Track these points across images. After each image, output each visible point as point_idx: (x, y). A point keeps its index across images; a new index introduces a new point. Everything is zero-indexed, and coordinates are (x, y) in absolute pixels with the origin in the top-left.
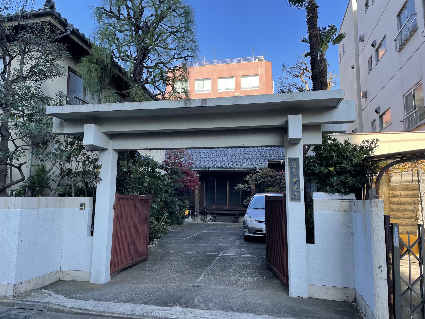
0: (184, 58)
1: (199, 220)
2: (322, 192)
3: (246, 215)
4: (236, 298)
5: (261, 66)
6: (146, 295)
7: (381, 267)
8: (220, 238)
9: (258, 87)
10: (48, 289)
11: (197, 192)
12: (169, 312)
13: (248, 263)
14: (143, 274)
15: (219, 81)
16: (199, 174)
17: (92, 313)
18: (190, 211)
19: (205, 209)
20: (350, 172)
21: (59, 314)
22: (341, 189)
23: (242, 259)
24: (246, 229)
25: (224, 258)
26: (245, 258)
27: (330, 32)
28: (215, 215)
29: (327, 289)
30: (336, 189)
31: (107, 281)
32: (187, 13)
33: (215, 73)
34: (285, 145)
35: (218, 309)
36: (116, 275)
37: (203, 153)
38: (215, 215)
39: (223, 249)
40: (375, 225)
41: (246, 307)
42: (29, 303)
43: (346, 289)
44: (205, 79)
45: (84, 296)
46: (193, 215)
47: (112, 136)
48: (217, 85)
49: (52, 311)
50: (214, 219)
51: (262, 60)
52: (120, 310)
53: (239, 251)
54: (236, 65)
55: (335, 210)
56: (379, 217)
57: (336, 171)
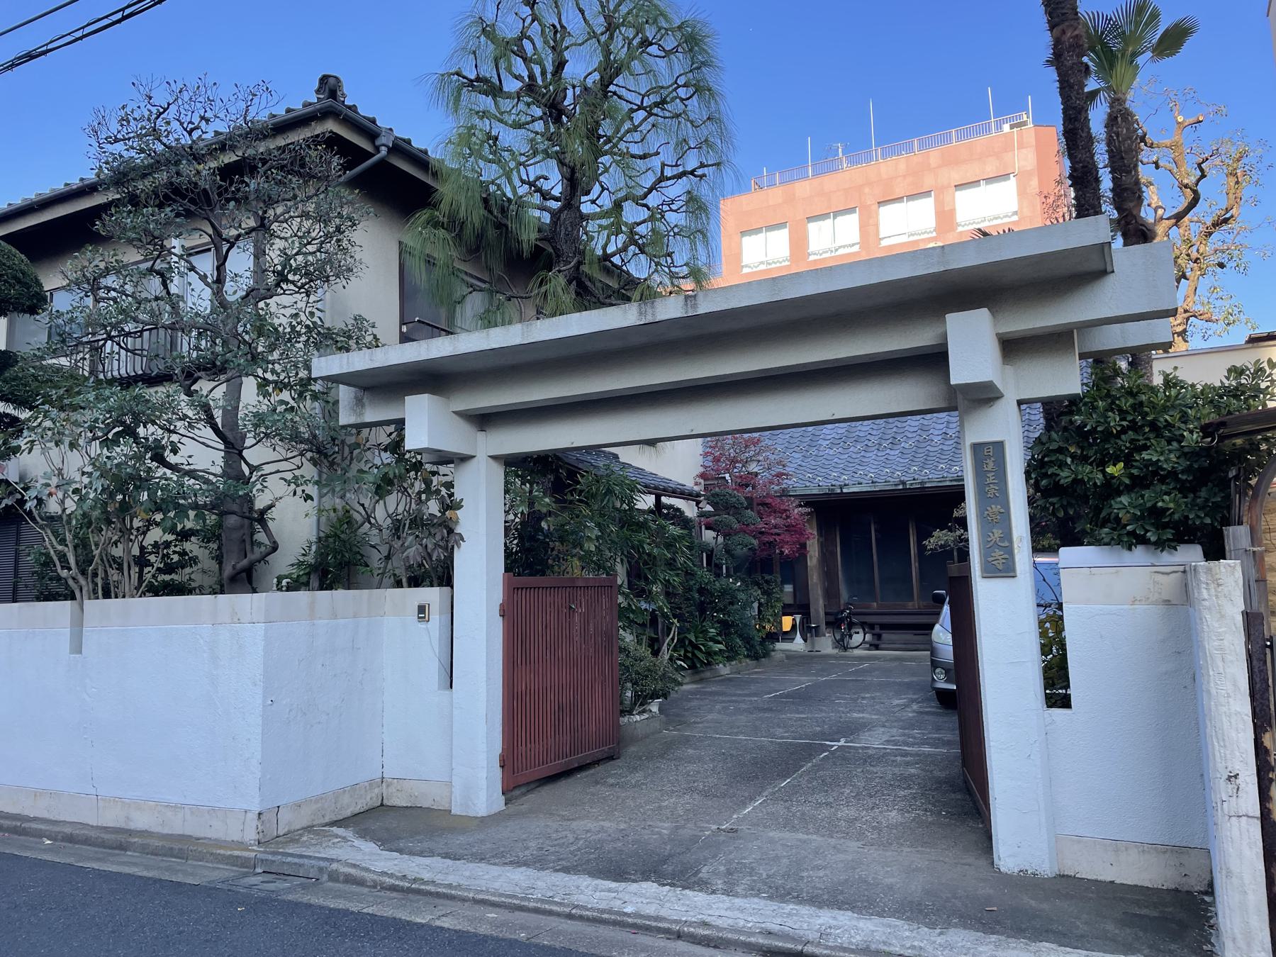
0: (692, 173)
1: (826, 644)
2: (1089, 544)
3: (937, 627)
4: (825, 868)
5: (1021, 146)
6: (579, 849)
7: (1236, 776)
8: (863, 698)
9: (1015, 213)
10: (346, 827)
12: (620, 895)
13: (913, 771)
14: (593, 795)
15: (884, 210)
16: (805, 506)
17: (428, 888)
18: (798, 617)
19: (842, 612)
20: (1173, 474)
21: (354, 888)
22: (1147, 531)
23: (899, 758)
24: (938, 670)
25: (843, 756)
26: (911, 755)
27: (1137, 24)
28: (877, 630)
29: (1117, 850)
30: (1129, 534)
32: (692, 41)
33: (867, 190)
35: (757, 896)
36: (524, 794)
38: (877, 630)
39: (851, 730)
40: (1211, 645)
41: (842, 893)
42: (290, 859)
43: (1180, 850)
44: (837, 214)
45: (426, 845)
46: (808, 630)
47: (484, 420)
48: (877, 225)
49: (337, 881)
50: (876, 642)
51: (1025, 123)
52: (497, 885)
53: (904, 735)
54: (934, 155)
55: (1133, 603)
56: (1223, 616)
57: (1131, 476)
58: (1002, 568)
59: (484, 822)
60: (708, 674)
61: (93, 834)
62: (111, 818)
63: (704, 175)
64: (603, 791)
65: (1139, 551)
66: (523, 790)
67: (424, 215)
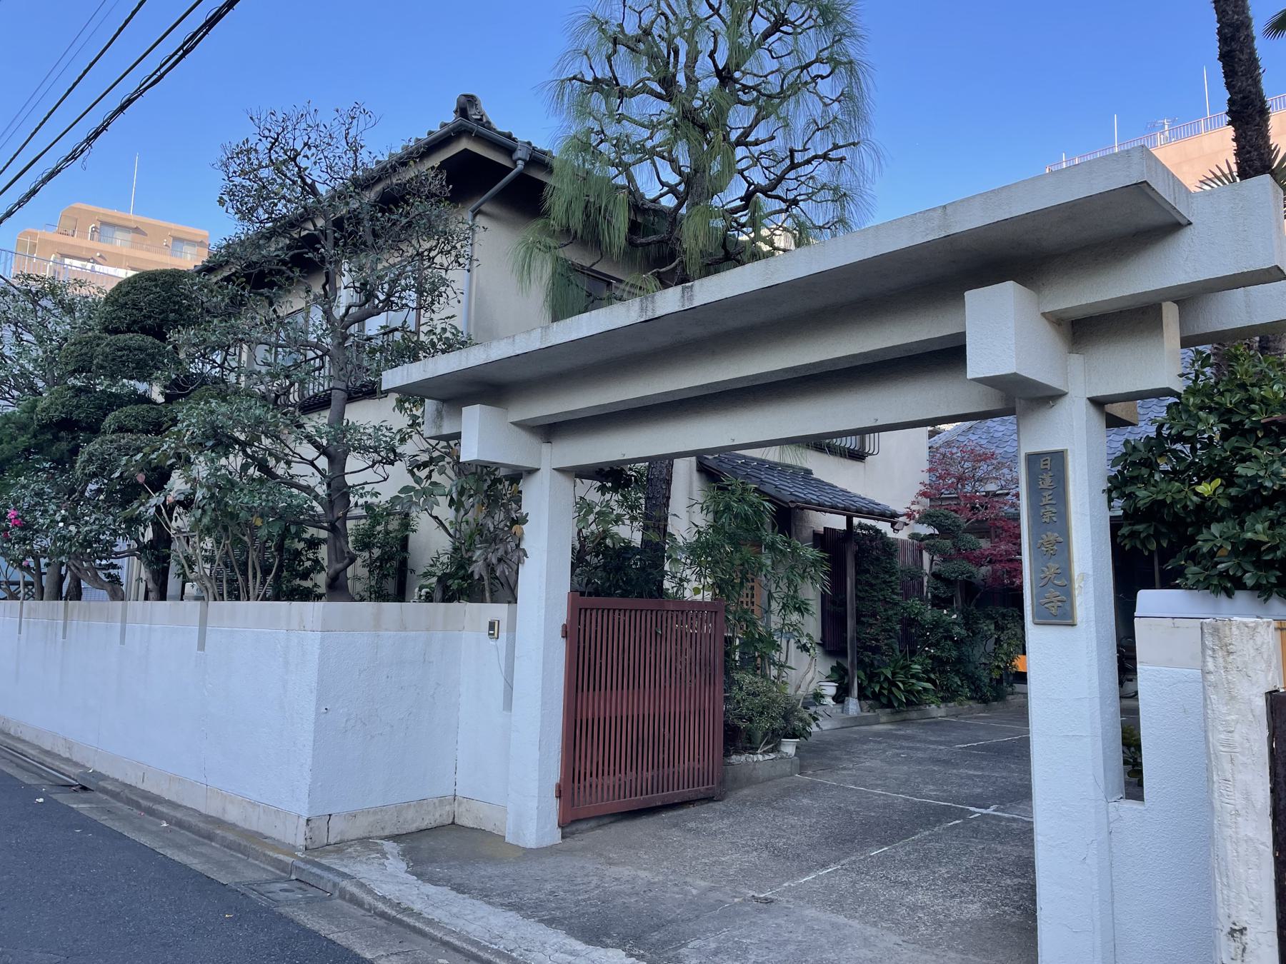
0: (825, 157)
30: (1220, 574)
31: (548, 842)
34: (1019, 405)
36: (592, 829)
47: (550, 430)
49: (344, 899)
52: (471, 928)
56: (1233, 698)
58: (1061, 615)
59: (528, 854)
60: (914, 715)
61: (193, 821)
62: (212, 809)
63: (842, 159)
64: (676, 835)
65: (1241, 596)
66: (592, 824)
67: (541, 222)
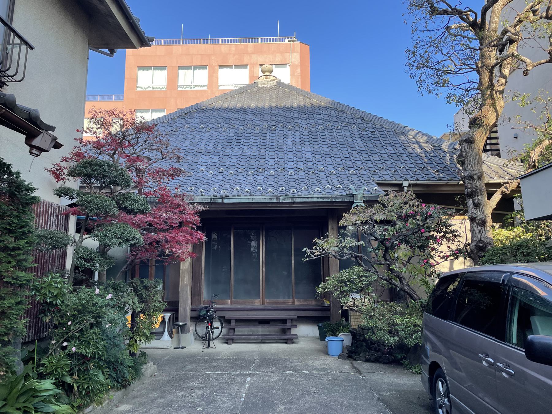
5: (293, 51)
11: (185, 266)
37: (202, 168)
44: (196, 67)
48: (217, 78)
54: (250, 46)
